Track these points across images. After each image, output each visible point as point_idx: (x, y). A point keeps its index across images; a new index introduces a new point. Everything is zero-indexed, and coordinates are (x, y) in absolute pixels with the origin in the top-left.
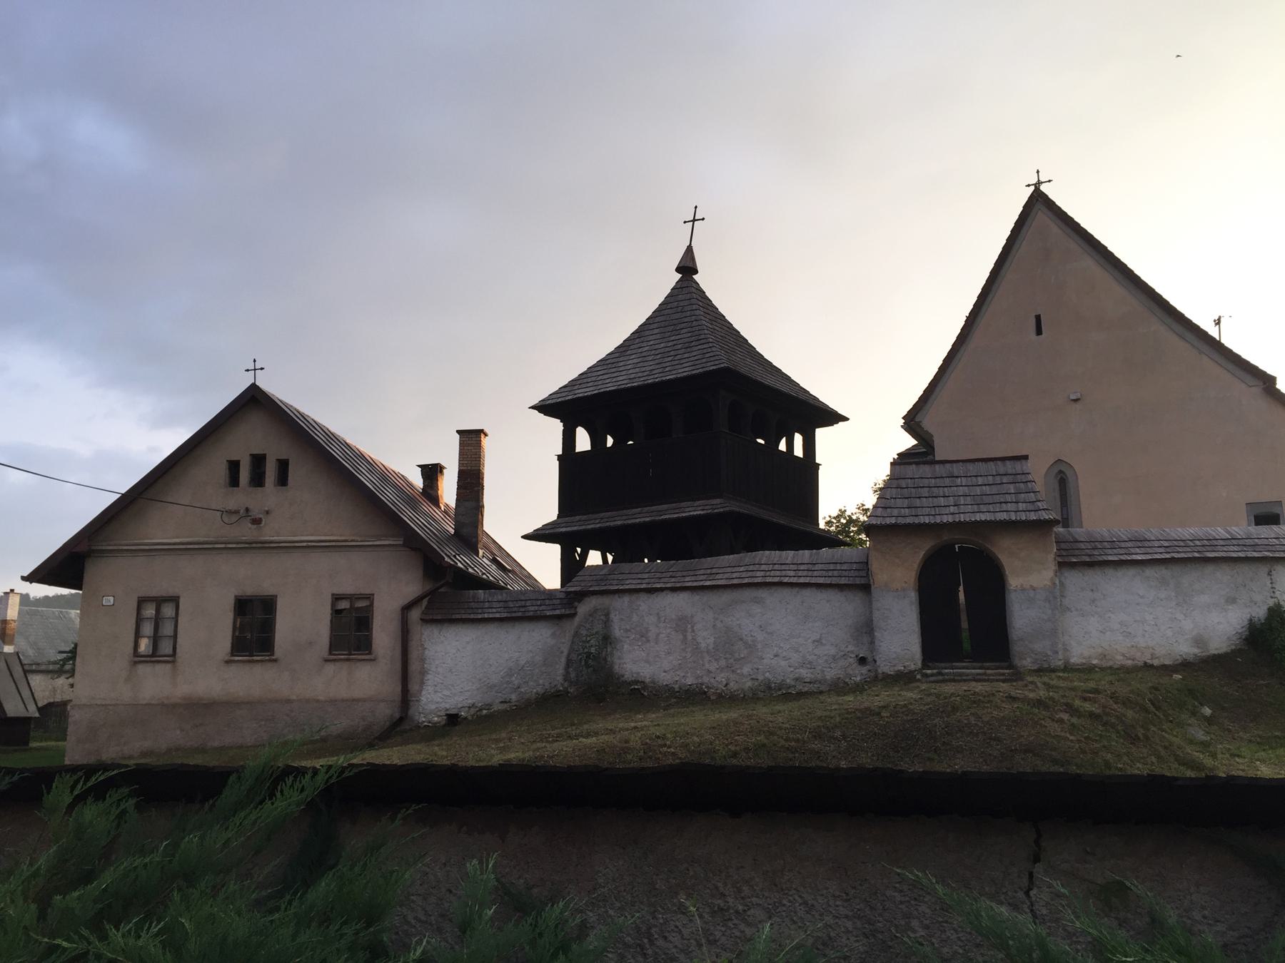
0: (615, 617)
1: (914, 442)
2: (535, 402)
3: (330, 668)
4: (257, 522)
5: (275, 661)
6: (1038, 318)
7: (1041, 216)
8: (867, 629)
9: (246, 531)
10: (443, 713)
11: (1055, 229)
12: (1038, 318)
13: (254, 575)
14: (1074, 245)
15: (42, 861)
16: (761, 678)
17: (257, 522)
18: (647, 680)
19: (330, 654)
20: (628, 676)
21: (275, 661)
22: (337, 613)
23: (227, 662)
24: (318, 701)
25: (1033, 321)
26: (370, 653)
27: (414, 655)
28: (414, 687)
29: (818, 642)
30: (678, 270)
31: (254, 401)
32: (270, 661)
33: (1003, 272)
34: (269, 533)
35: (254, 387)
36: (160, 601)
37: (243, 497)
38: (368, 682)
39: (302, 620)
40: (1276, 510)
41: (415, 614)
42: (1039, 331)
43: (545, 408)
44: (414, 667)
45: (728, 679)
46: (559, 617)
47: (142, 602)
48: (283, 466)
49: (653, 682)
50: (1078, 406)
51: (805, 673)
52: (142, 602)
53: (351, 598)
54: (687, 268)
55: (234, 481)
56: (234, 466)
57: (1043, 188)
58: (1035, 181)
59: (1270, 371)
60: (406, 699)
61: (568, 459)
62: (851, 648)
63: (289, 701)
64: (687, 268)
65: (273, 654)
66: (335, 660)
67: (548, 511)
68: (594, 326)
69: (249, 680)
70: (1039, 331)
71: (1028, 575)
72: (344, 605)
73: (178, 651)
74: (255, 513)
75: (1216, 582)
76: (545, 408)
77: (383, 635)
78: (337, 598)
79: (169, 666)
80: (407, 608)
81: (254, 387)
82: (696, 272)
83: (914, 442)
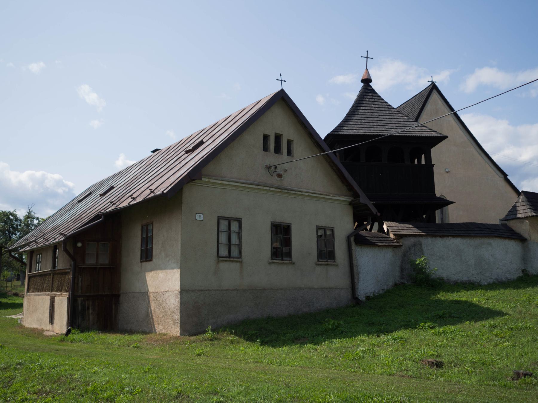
3: (318, 269)
4: (280, 176)
5: (294, 263)
9: (275, 180)
11: (440, 102)
13: (283, 210)
16: (494, 278)
17: (280, 176)
18: (445, 279)
19: (318, 261)
20: (433, 276)
22: (319, 237)
23: (270, 264)
31: (281, 99)
34: (288, 181)
35: (282, 91)
36: (230, 220)
37: (272, 159)
38: (335, 277)
39: (303, 241)
41: (352, 239)
46: (395, 247)
47: (220, 219)
50: (448, 174)
51: (508, 276)
52: (220, 219)
53: (325, 229)
54: (367, 81)
55: (266, 148)
56: (266, 138)
59: (507, 173)
63: (300, 289)
64: (367, 81)
69: (280, 276)
73: (243, 254)
74: (279, 171)
78: (319, 228)
79: (238, 264)
81: (282, 91)
82: (371, 81)
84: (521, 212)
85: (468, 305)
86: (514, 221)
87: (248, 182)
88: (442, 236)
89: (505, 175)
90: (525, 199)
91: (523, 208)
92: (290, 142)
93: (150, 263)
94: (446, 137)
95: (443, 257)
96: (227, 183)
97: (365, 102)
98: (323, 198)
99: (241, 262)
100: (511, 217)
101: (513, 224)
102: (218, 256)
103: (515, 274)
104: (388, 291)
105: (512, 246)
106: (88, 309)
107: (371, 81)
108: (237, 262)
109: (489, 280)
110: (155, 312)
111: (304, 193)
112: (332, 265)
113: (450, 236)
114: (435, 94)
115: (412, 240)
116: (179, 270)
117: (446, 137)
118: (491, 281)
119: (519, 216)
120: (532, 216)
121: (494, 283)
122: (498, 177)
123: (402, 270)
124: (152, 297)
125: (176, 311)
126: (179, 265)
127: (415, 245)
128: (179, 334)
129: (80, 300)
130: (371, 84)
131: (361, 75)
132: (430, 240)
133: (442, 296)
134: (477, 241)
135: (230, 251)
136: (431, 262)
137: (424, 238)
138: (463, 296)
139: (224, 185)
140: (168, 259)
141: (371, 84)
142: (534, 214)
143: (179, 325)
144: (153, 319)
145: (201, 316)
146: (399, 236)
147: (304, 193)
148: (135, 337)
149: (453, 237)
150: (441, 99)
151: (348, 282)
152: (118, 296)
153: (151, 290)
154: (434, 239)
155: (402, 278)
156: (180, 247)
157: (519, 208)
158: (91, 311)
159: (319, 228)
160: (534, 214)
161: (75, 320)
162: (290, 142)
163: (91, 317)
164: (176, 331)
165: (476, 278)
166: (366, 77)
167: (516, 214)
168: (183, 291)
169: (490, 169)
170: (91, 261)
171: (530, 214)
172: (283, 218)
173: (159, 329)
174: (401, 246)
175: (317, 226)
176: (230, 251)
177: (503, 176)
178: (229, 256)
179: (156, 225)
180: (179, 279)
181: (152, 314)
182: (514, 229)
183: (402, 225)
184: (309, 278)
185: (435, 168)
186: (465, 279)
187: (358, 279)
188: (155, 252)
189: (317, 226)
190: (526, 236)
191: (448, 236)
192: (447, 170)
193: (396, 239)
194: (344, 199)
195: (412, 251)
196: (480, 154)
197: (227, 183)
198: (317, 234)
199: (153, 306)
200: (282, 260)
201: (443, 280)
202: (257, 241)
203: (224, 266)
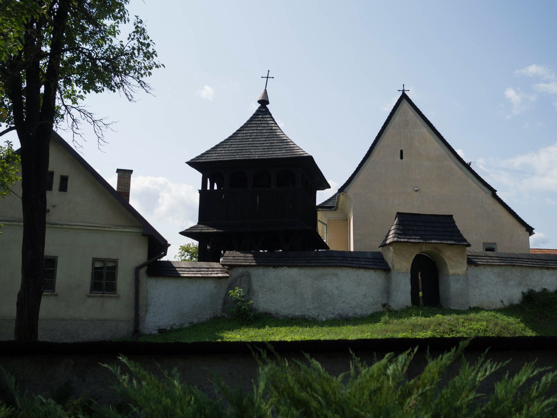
0: (254, 280)
1: (317, 204)
2: (189, 160)
3: (90, 301)
5: (56, 295)
6: (402, 152)
7: (405, 103)
8: (387, 291)
10: (157, 328)
12: (402, 152)
14: (419, 121)
15: (244, 401)
16: (336, 313)
19: (91, 293)
20: (261, 310)
21: (56, 295)
22: (95, 269)
24: (82, 320)
25: (399, 152)
26: (115, 294)
27: (141, 296)
28: (142, 313)
29: (365, 296)
30: (259, 102)
32: (52, 295)
33: (387, 128)
40: (494, 246)
41: (143, 271)
42: (402, 158)
43: (193, 164)
44: (141, 302)
45: (319, 313)
48: (64, 180)
49: (277, 314)
50: (417, 193)
54: (264, 102)
57: (406, 92)
58: (402, 89)
60: (137, 320)
61: (203, 193)
62: (379, 299)
64: (264, 102)
65: (54, 291)
66: (94, 296)
67: (192, 221)
68: (218, 124)
70: (402, 158)
71: (455, 267)
72: (98, 265)
75: (515, 274)
76: (193, 164)
77: (124, 281)
78: (95, 260)
80: (137, 269)
82: (268, 103)
83: (317, 204)
98: (85, 229)
104: (203, 324)
107: (268, 103)
109: (330, 316)
111: (73, 227)
112: (109, 297)
113: (285, 266)
115: (241, 270)
122: (484, 193)
127: (241, 276)
131: (259, 97)
132: (261, 270)
134: (319, 271)
136: (260, 295)
137: (254, 268)
141: (267, 106)
147: (73, 227)
149: (289, 267)
150: (413, 109)
151: (132, 314)
154: (265, 269)
155: (223, 311)
165: (313, 313)
169: (474, 185)
175: (93, 258)
177: (490, 192)
179: (147, 260)
187: (146, 311)
189: (93, 258)
191: (282, 266)
192: (416, 189)
194: (132, 231)
195: (238, 283)
196: (460, 168)
198: (93, 266)
201: (271, 314)
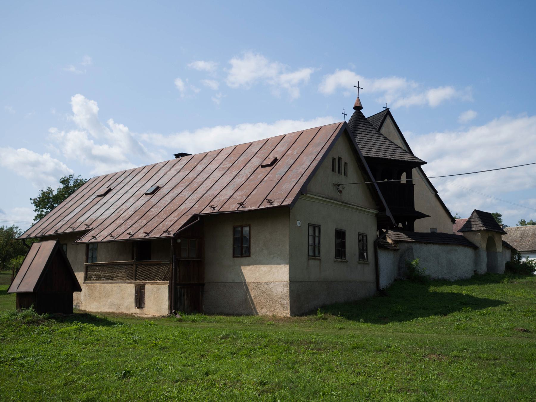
4: (340, 192)
22: (360, 241)
23: (335, 262)
36: (314, 227)
39: (352, 245)
47: (309, 225)
52: (309, 225)
56: (334, 159)
74: (340, 188)
82: (361, 108)
84: (475, 226)
85: (459, 296)
86: (469, 233)
87: (324, 196)
88: (426, 243)
89: (436, 192)
90: (477, 216)
91: (477, 223)
92: (346, 164)
93: (248, 258)
94: (426, 163)
95: (429, 260)
96: (315, 197)
97: (360, 127)
99: (320, 260)
100: (466, 229)
101: (469, 236)
102: (309, 255)
103: (470, 274)
105: (469, 252)
106: (184, 295)
108: (318, 259)
109: (455, 278)
110: (256, 298)
114: (388, 119)
115: (406, 245)
116: (288, 266)
117: (426, 163)
118: (457, 279)
119: (474, 229)
120: (484, 230)
121: (458, 280)
123: (399, 268)
124: (251, 287)
125: (284, 297)
126: (288, 261)
128: (289, 315)
129: (178, 287)
130: (361, 111)
133: (432, 289)
134: (449, 248)
135: (314, 252)
138: (446, 289)
139: (312, 198)
140: (272, 256)
141: (361, 111)
142: (485, 228)
143: (289, 308)
144: (253, 304)
145: (305, 300)
146: (396, 242)
148: (241, 318)
149: (434, 244)
152: (203, 285)
153: (248, 280)
156: (288, 247)
157: (473, 223)
158: (185, 297)
159: (359, 235)
160: (485, 228)
161: (176, 303)
162: (346, 164)
163: (186, 302)
164: (286, 312)
166: (358, 105)
167: (471, 228)
168: (292, 281)
170: (184, 255)
171: (482, 228)
172: (342, 226)
173: (262, 311)
174: (398, 250)
175: (359, 233)
176: (314, 252)
178: (315, 256)
180: (288, 272)
181: (252, 300)
182: (468, 239)
183: (396, 233)
184: (356, 275)
185: (415, 188)
186: (440, 277)
188: (252, 250)
189: (359, 233)
190: (478, 245)
191: (430, 243)
193: (394, 244)
197: (315, 197)
199: (253, 293)
200: (341, 259)
202: (328, 244)
203: (312, 262)
